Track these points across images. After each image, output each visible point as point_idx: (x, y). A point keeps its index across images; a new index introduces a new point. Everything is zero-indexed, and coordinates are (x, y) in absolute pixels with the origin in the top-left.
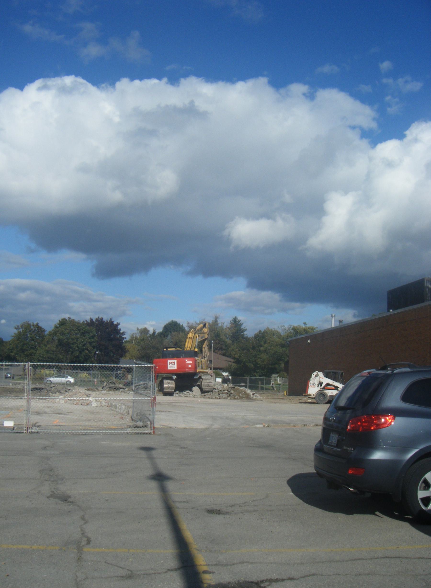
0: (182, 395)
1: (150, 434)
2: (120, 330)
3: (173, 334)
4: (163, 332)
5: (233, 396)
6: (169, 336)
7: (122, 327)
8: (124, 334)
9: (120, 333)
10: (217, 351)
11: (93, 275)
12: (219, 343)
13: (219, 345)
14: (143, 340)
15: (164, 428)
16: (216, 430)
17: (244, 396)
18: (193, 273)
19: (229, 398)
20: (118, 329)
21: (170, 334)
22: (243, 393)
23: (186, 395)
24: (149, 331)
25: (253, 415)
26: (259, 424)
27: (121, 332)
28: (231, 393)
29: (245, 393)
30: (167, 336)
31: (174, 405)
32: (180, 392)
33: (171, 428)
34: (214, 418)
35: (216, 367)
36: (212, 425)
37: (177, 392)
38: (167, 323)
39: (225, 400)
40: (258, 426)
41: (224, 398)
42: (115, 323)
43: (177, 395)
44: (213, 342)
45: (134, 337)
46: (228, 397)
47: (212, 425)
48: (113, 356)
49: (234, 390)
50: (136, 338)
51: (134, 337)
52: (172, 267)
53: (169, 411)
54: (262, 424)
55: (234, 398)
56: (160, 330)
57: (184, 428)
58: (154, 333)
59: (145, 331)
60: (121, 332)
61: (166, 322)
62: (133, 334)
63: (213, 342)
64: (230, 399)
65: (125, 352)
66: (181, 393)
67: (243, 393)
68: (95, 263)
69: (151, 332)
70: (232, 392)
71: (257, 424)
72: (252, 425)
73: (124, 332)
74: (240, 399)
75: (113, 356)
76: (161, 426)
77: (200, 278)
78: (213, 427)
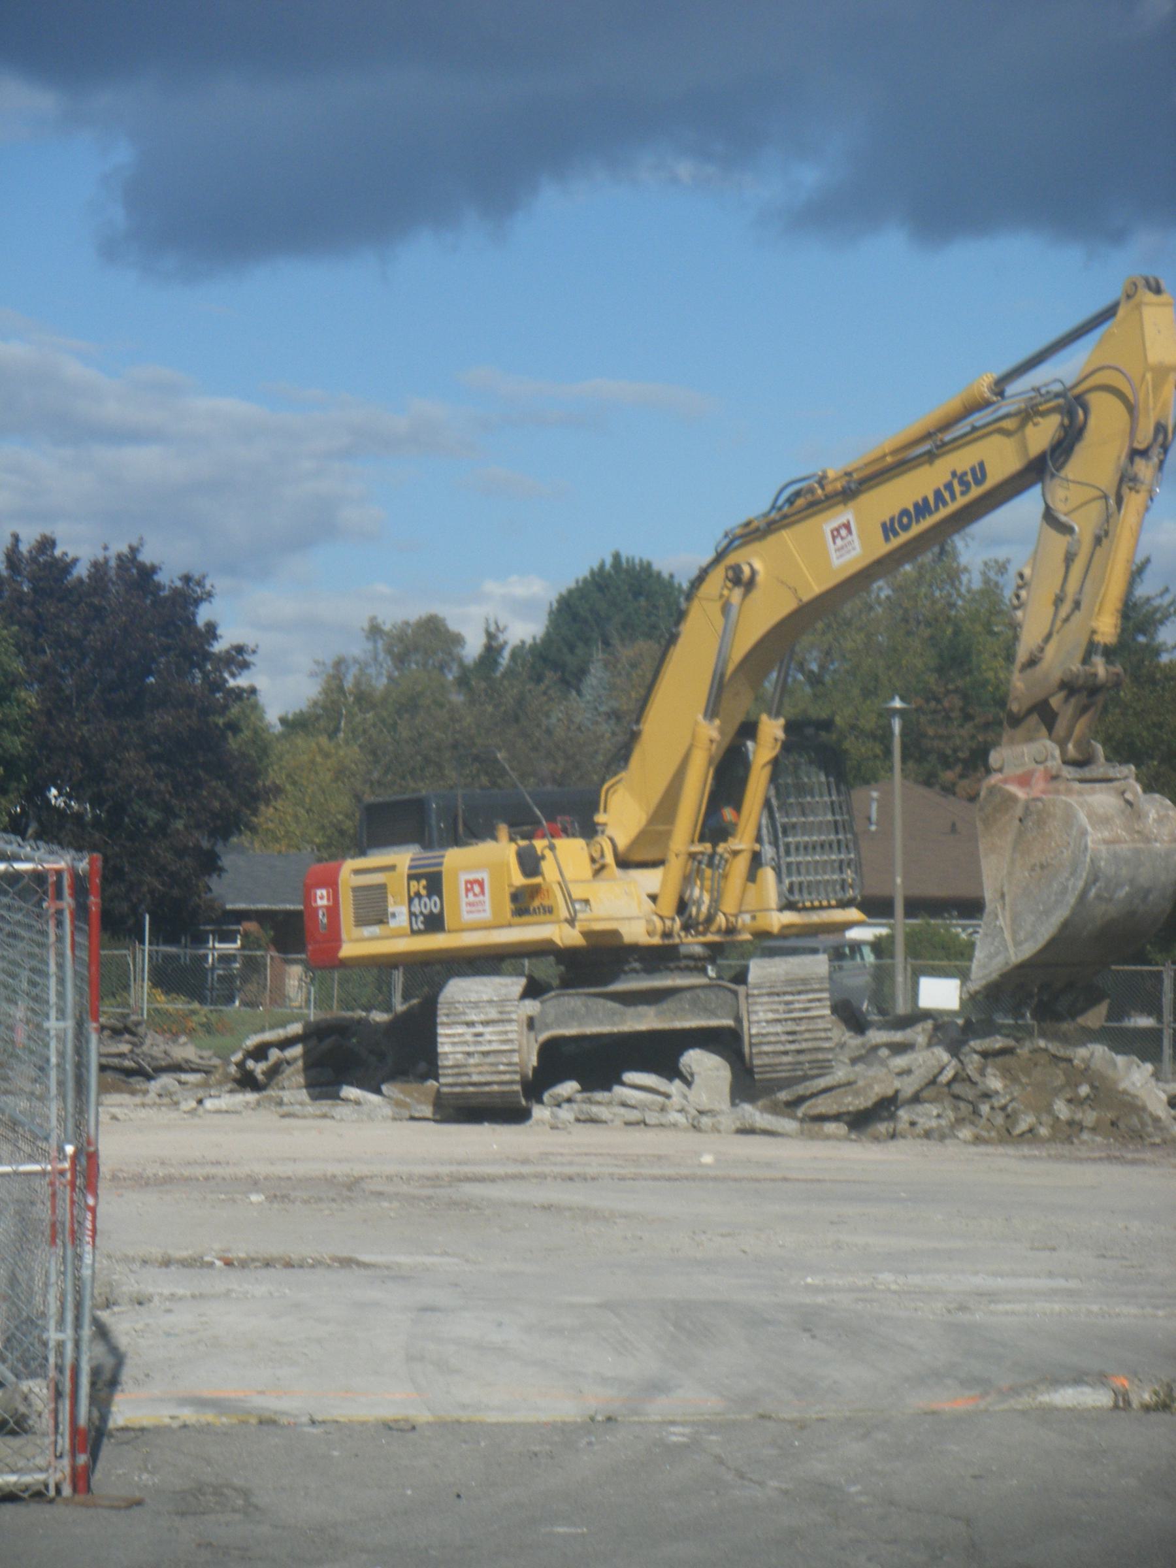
0: (603, 1112)
1: (38, 1495)
2: (211, 631)
3: (626, 653)
4: (548, 640)
5: (999, 1120)
6: (596, 675)
7: (230, 618)
8: (245, 665)
9: (207, 656)
10: (949, 776)
11: (110, 250)
12: (968, 717)
13: (969, 726)
14: (410, 705)
15: (205, 1429)
16: (677, 1435)
17: (1089, 1117)
18: (836, 214)
19: (966, 1133)
20: (191, 622)
21: (599, 655)
22: (1084, 1090)
23: (634, 1115)
24: (458, 640)
25: (1053, 1293)
26: (1078, 1379)
27: (218, 647)
28: (987, 1095)
29: (1104, 1094)
30: (583, 672)
31: (453, 1204)
32: (586, 1087)
33: (268, 1422)
34: (688, 1324)
35: (933, 890)
36: (656, 1387)
37: (569, 1087)
38: (583, 572)
39: (933, 1148)
40: (1066, 1397)
41: (928, 1134)
42: (168, 578)
43: (566, 1114)
44: (897, 704)
45: (349, 684)
46: (960, 1121)
47: (656, 1387)
48: (162, 829)
49: (1007, 1073)
50: (363, 698)
51: (349, 684)
52: (685, 169)
53: (347, 1263)
54: (1101, 1379)
55: (1008, 1136)
56: (525, 630)
57: (388, 1426)
58: (492, 651)
59: (431, 637)
60: (218, 647)
61: (573, 570)
62: (339, 663)
63: (897, 704)
64: (978, 1140)
65: (254, 799)
66: (600, 1096)
67: (1084, 1090)
68: (123, 154)
69: (473, 647)
70: (995, 1083)
71: (1056, 1382)
72: (1015, 1391)
73: (240, 649)
74: (1052, 1139)
75: (162, 829)
76: (188, 1415)
77: (889, 251)
78: (657, 1408)
